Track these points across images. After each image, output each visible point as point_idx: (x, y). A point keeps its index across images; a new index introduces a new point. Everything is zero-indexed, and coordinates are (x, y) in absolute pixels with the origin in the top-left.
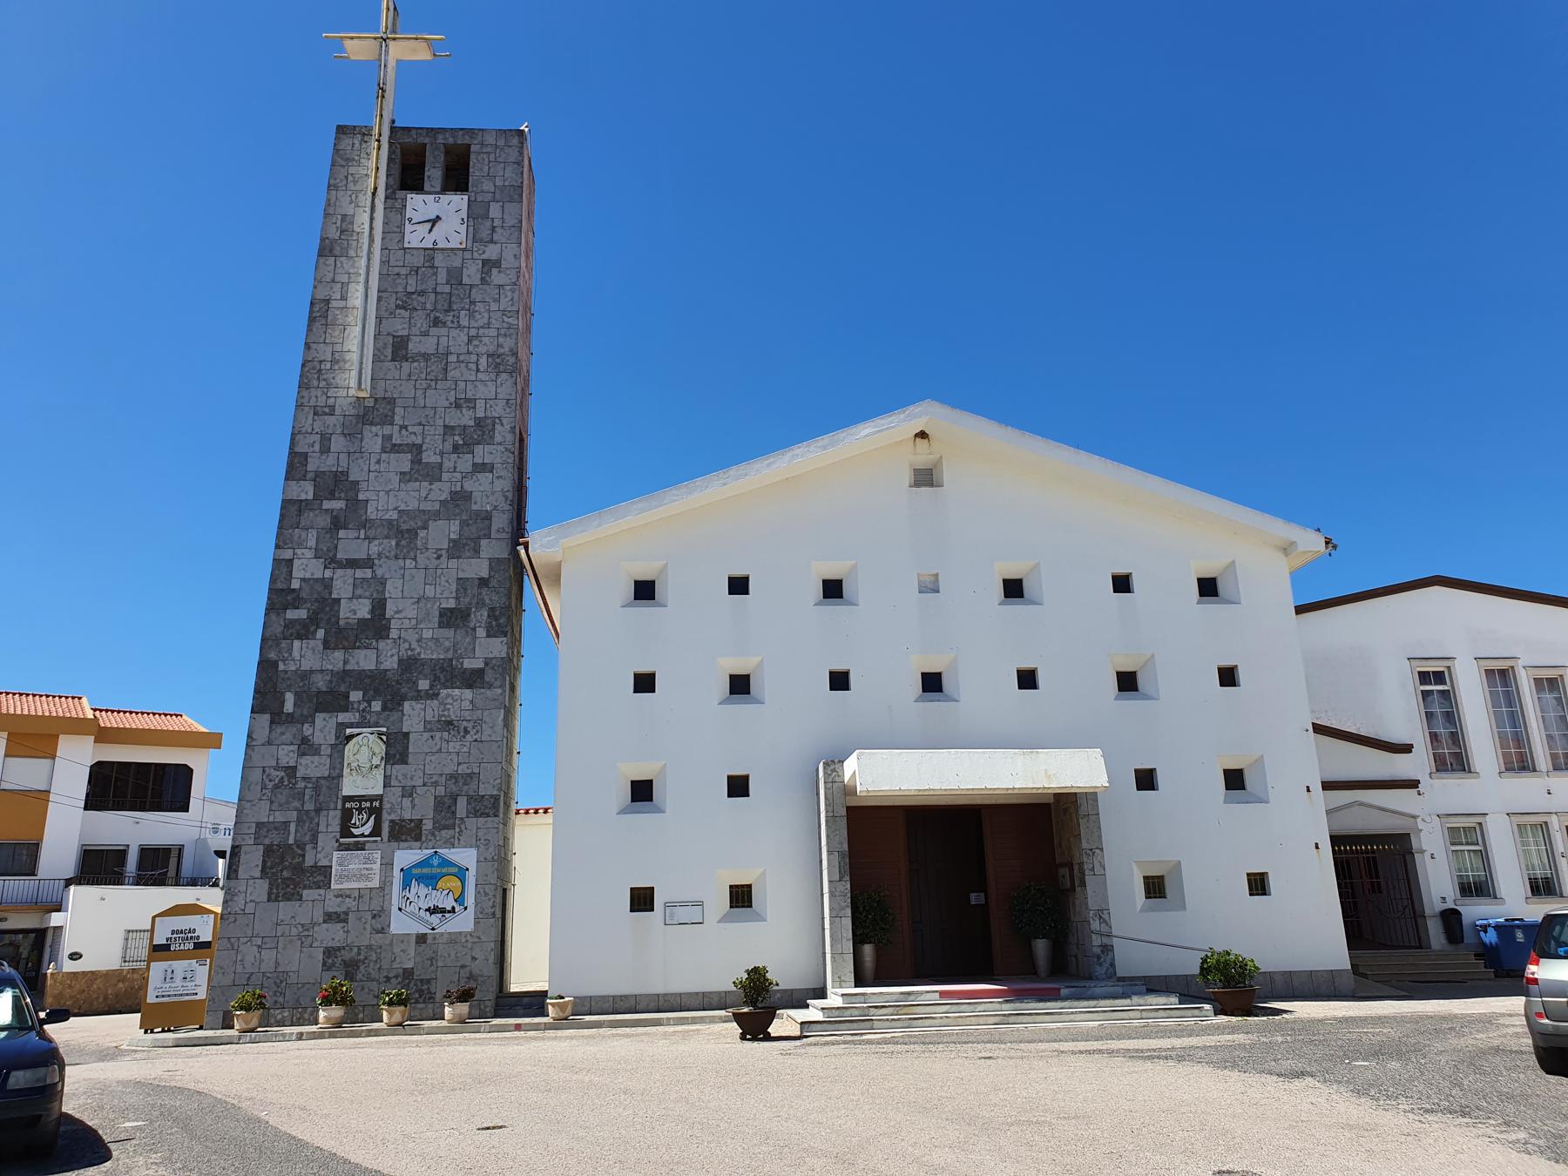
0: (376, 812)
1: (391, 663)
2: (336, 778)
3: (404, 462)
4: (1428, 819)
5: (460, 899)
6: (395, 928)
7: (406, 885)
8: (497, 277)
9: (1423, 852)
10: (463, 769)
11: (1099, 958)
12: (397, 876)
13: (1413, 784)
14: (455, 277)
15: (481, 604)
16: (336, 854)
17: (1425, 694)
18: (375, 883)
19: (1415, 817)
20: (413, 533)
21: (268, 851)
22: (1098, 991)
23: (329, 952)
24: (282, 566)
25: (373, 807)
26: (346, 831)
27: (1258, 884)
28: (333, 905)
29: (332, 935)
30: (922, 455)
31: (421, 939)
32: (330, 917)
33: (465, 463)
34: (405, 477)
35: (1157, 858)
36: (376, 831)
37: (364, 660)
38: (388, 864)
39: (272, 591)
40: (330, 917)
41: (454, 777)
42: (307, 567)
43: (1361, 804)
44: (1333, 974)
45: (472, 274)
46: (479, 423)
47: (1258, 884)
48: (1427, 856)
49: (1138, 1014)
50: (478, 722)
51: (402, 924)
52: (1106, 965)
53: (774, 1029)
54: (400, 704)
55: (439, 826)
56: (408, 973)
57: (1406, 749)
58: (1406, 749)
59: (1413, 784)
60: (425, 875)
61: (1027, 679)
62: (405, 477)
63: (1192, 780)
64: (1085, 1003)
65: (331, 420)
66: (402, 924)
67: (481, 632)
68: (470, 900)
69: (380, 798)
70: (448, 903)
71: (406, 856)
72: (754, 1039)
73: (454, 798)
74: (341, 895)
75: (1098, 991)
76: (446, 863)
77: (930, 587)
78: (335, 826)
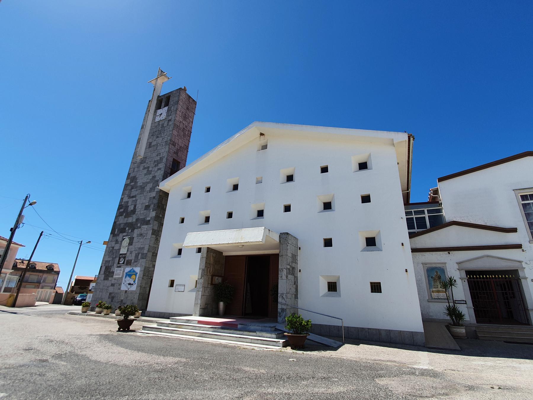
0: (125, 258)
1: (134, 220)
2: (120, 249)
3: (145, 171)
4: (528, 263)
5: (134, 281)
6: (122, 289)
7: (126, 277)
8: (170, 123)
9: (526, 278)
10: (142, 246)
11: (280, 314)
12: (125, 274)
13: (519, 246)
14: (163, 126)
15: (153, 203)
16: (116, 269)
17: (524, 206)
18: (121, 276)
19: (520, 262)
20: (144, 187)
21: (106, 268)
22: (252, 328)
23: (110, 294)
24: (122, 199)
25: (124, 256)
26: (119, 263)
27: (376, 288)
28: (113, 282)
29: (111, 289)
30: (262, 141)
31: (126, 291)
32: (113, 285)
33: (156, 169)
34: (146, 175)
35: (333, 275)
36: (123, 263)
37: (130, 220)
38: (124, 271)
39: (119, 205)
40: (113, 285)
41: (140, 248)
42: (126, 199)
43: (488, 256)
44: (413, 334)
45: (165, 125)
46: (160, 158)
47: (376, 288)
48: (529, 280)
49: (250, 341)
50: (147, 234)
51: (124, 288)
52: (283, 317)
53: (131, 328)
54: (134, 230)
55: (135, 262)
56: (122, 301)
57: (514, 230)
58: (514, 230)
59: (519, 246)
60: (129, 275)
61: (287, 209)
62: (146, 175)
63: (350, 242)
64: (238, 332)
65: (136, 165)
66: (124, 288)
67: (151, 210)
68: (136, 282)
69: (126, 254)
70: (132, 282)
71: (128, 269)
72: (124, 331)
73: (139, 254)
74: (115, 279)
75: (252, 328)
76: (134, 271)
77: (259, 182)
78: (117, 262)
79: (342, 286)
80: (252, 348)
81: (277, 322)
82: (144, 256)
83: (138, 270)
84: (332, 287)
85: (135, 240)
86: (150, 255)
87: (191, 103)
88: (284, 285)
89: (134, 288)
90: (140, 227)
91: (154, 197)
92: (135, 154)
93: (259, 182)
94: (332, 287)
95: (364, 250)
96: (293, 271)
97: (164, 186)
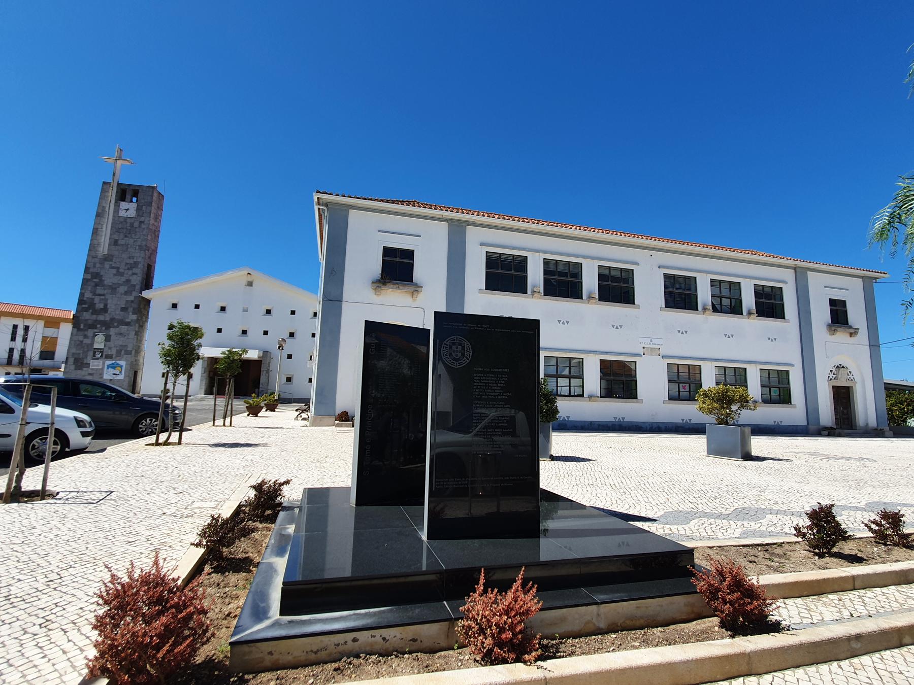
1: (108, 319)
3: (114, 271)
14: (132, 225)
25: (101, 351)
28: (90, 372)
33: (130, 272)
34: (115, 275)
42: (88, 295)
45: (136, 224)
61: (266, 333)
62: (115, 275)
75: (597, 598)
79: (294, 380)
80: (107, 209)
81: (33, 381)
82: (128, 353)
83: (123, 363)
84: (289, 380)
85: (113, 337)
86: (133, 352)
87: (161, 197)
88: (263, 379)
89: (121, 377)
90: (117, 327)
91: (132, 302)
92: (93, 247)
93: (245, 310)
94: (289, 380)
95: (480, 291)
96: (268, 371)
97: (146, 294)
